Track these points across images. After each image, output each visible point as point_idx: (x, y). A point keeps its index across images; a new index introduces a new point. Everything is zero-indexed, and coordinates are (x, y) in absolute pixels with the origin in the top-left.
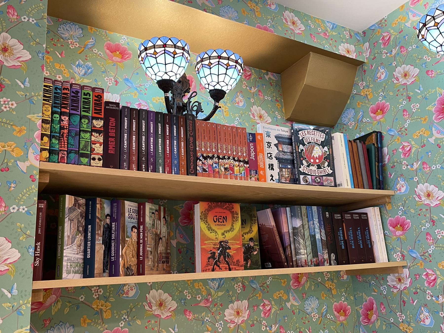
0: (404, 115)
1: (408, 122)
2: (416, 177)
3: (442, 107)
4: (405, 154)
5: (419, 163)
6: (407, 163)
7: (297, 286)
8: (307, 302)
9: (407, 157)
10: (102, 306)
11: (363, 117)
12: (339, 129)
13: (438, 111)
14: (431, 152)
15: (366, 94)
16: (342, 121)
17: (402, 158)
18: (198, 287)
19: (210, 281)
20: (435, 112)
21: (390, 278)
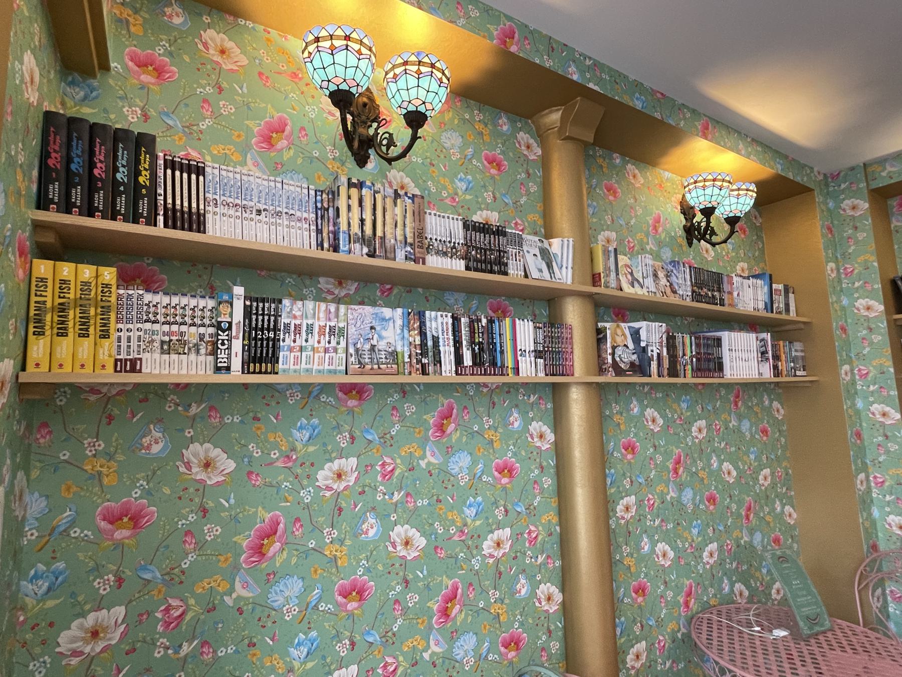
0: (394, 609)
1: (190, 558)
2: (191, 430)
5: (402, 493)
6: (168, 643)
11: (320, 599)
12: (446, 669)
13: (252, 548)
14: (223, 622)
15: (335, 556)
16: (269, 601)
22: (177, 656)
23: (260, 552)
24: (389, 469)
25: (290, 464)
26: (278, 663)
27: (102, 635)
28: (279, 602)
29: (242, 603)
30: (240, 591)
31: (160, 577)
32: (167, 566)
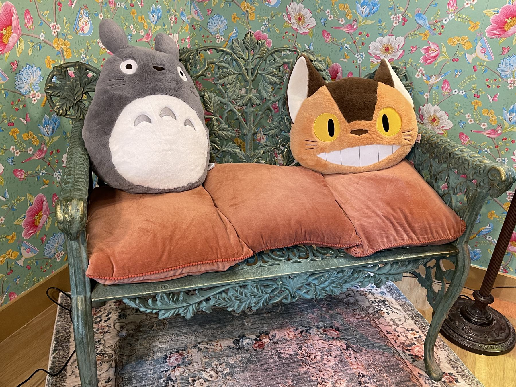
1: (450, 17)
2: (428, 94)
3: (504, 19)
4: (426, 59)
5: (440, 78)
8: (507, 61)
9: (428, 64)
10: (248, 8)
16: (498, 69)
17: (420, 63)
20: (492, 22)
21: (375, 45)
23: (502, 28)
25: (351, 31)
26: (492, 117)
27: (390, 51)
28: (507, 73)
29: (478, 63)
31: (428, 25)
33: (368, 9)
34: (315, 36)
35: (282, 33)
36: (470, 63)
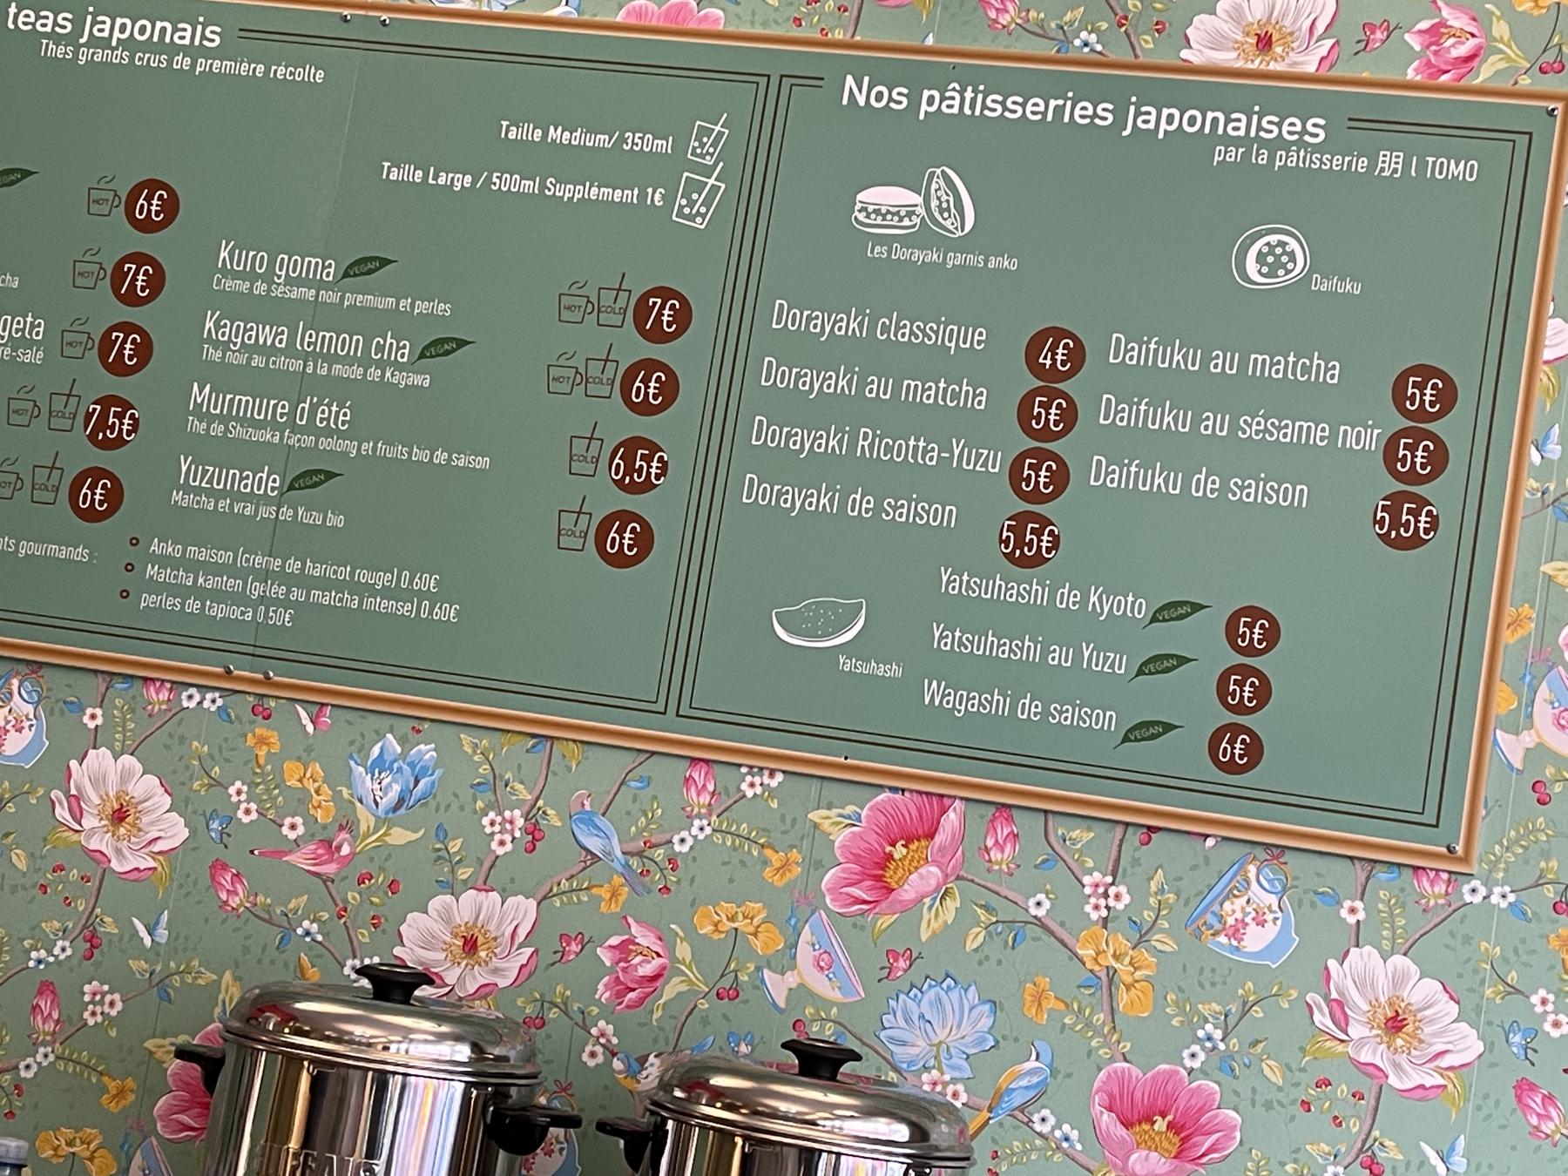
7: (865, 902)
8: (911, 1005)
10: (1116, 957)
16: (883, 1035)
18: (300, 781)
19: (361, 769)
21: (421, 927)
22: (630, 1084)
24: (647, 970)
28: (915, 1051)
29: (809, 1011)
30: (806, 971)
31: (619, 854)
32: (640, 832)
33: (397, 788)
34: (1479, 1108)
35: (1297, 1085)
36: (781, 1011)
